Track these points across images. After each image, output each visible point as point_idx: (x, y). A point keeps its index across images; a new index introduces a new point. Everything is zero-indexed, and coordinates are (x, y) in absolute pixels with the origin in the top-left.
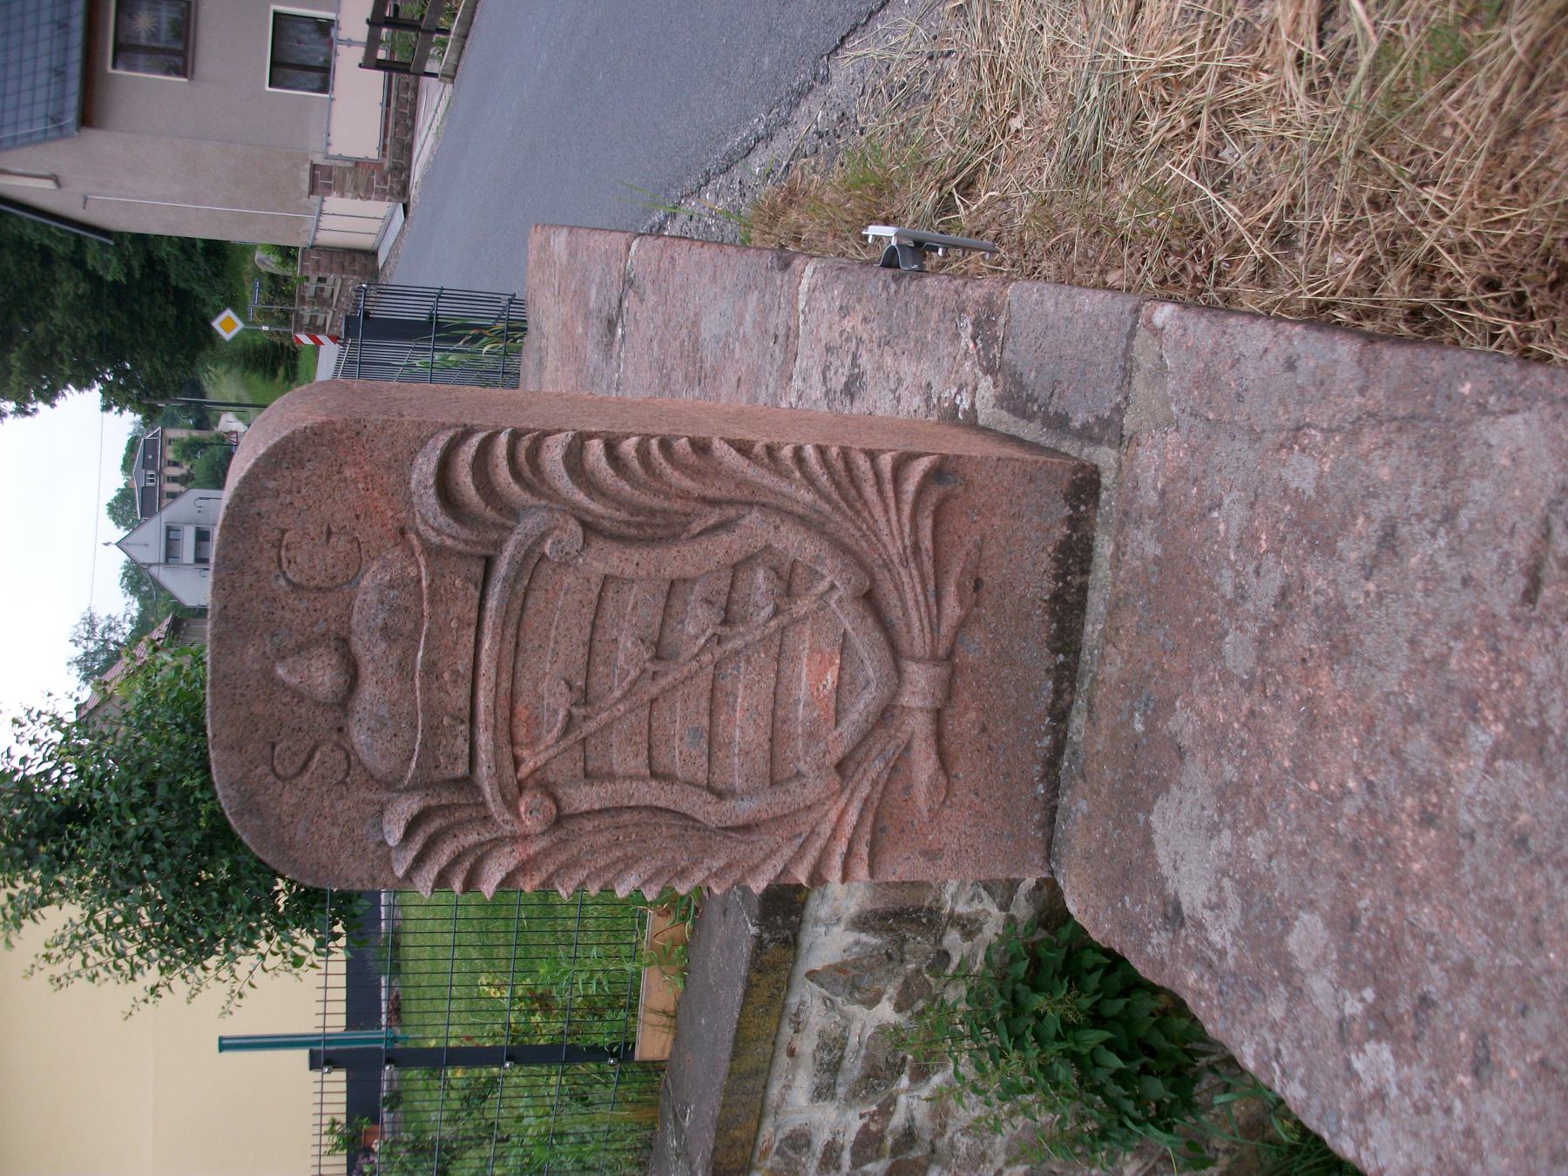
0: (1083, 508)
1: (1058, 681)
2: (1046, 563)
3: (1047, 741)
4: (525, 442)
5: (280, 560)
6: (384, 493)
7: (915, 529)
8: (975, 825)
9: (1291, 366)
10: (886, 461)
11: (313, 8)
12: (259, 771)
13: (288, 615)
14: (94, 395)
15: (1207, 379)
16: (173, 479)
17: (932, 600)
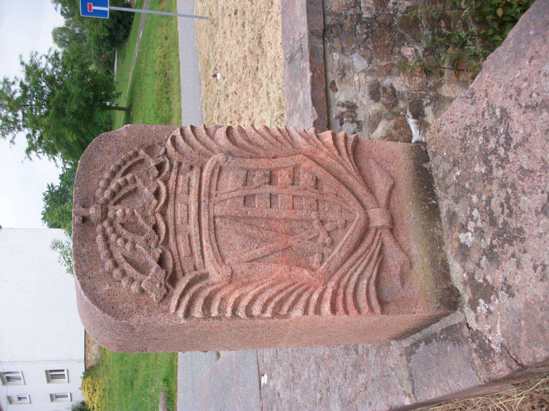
9: (370, 404)
14: (61, 22)
15: (388, 388)
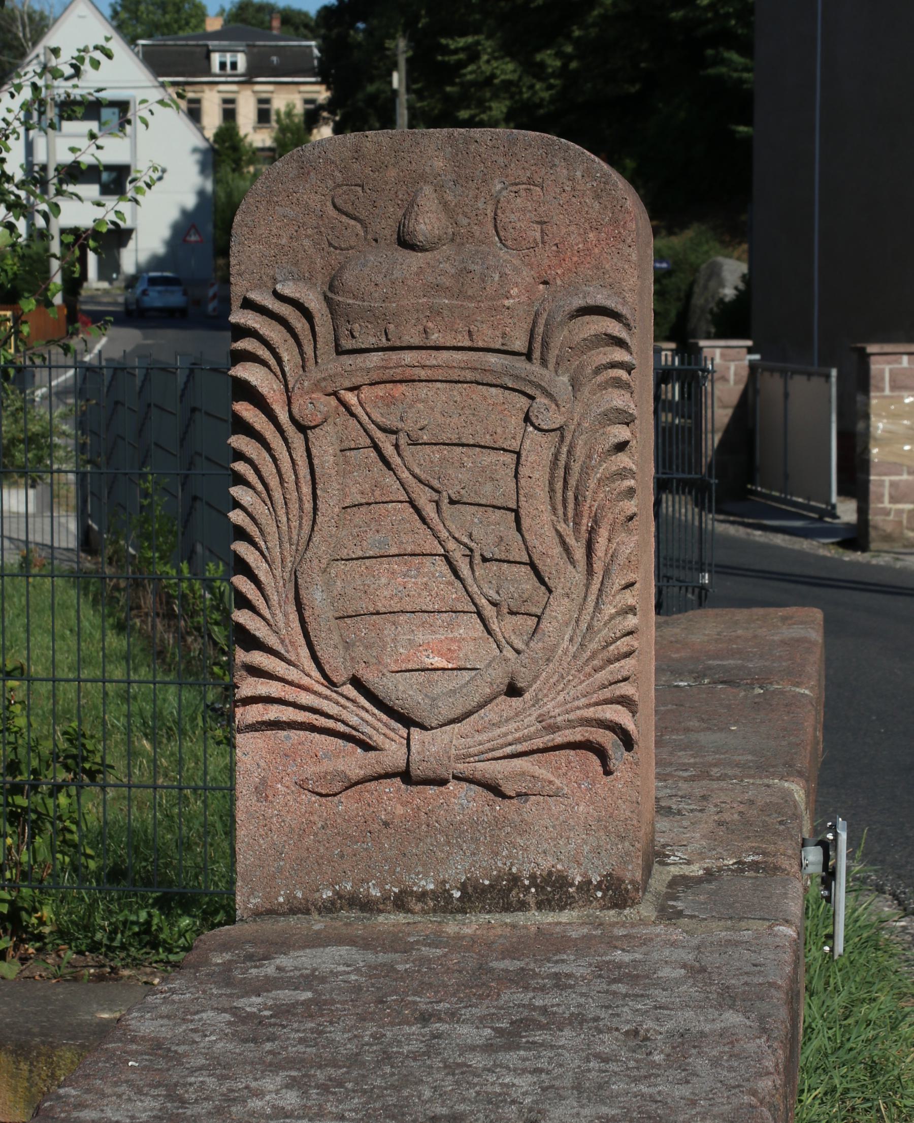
0: (599, 894)
1: (434, 895)
2: (546, 864)
3: (375, 893)
4: (622, 374)
5: (516, 184)
6: (577, 265)
7: (571, 724)
8: (292, 830)
10: (626, 689)
11: (830, 401)
12: (337, 173)
13: (471, 194)
16: (229, 114)
17: (509, 750)
